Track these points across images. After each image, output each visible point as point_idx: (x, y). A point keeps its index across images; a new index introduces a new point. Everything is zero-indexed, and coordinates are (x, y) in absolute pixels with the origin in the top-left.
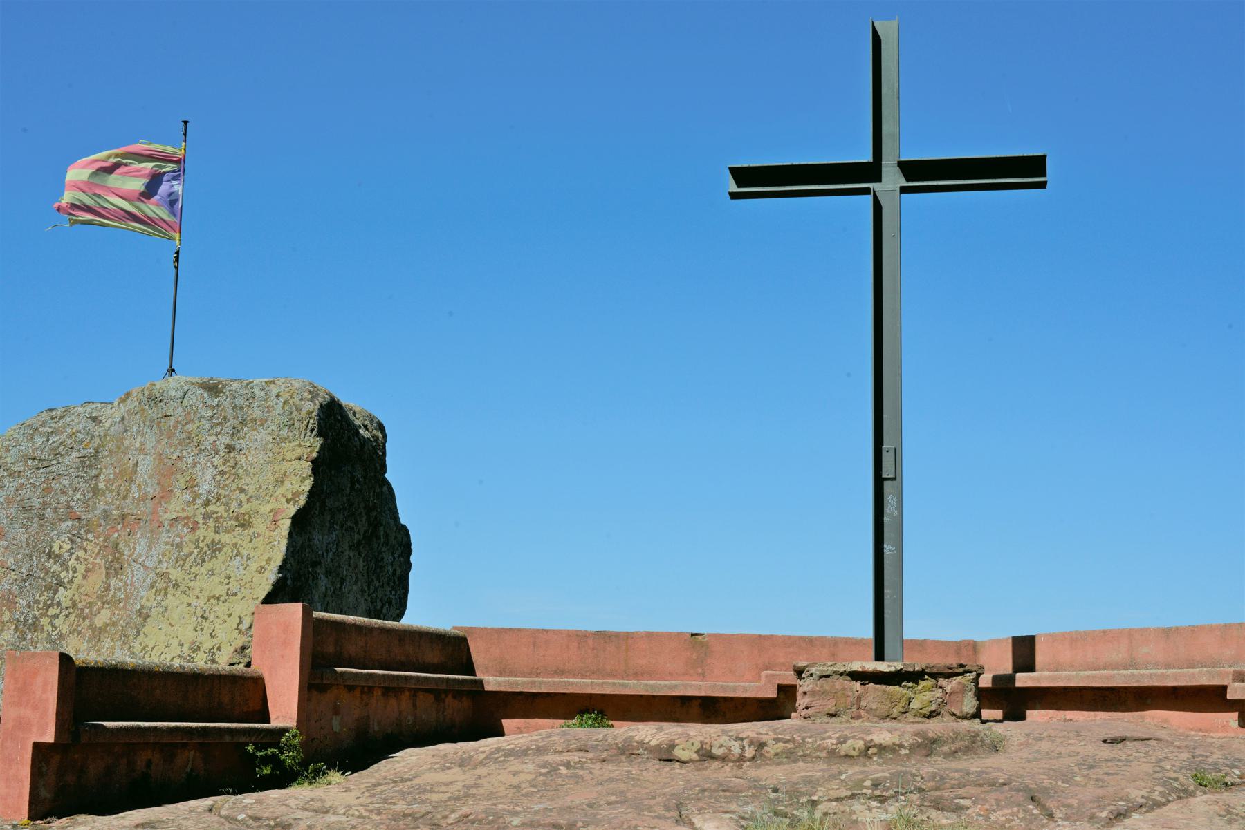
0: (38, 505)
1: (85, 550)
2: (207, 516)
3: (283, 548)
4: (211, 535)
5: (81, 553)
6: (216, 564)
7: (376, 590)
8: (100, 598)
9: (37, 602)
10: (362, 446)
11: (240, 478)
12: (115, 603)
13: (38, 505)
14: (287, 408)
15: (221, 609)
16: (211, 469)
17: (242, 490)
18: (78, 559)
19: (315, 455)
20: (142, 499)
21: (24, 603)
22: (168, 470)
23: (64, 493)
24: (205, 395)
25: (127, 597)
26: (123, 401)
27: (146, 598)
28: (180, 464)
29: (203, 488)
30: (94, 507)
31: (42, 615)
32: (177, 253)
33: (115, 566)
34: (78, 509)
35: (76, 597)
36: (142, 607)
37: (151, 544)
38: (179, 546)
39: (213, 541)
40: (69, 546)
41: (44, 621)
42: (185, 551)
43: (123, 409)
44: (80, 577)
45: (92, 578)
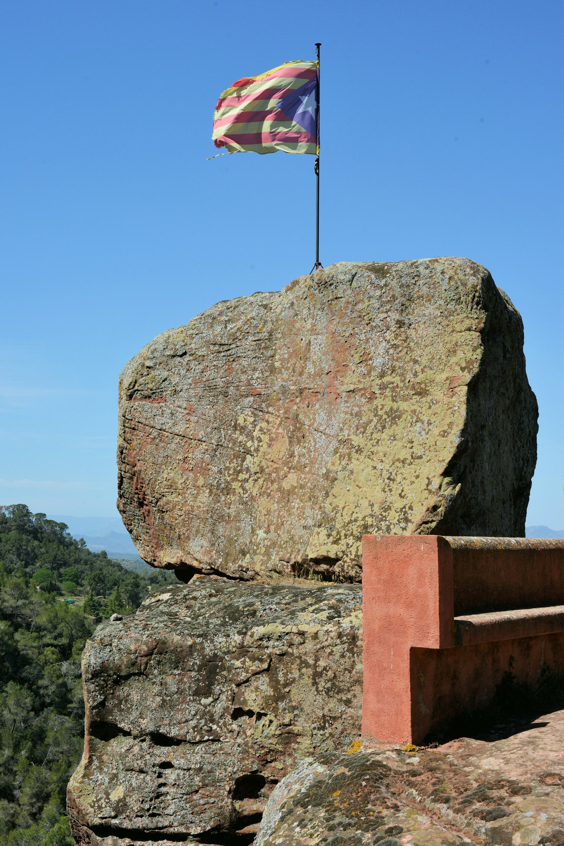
0: (221, 384)
1: (268, 422)
2: (383, 387)
3: (464, 413)
4: (389, 404)
5: (264, 425)
6: (398, 429)
7: (519, 450)
8: (286, 463)
9: (227, 468)
10: (510, 318)
11: (412, 350)
12: (300, 468)
13: (221, 384)
14: (452, 283)
15: (407, 471)
16: (384, 344)
17: (416, 362)
18: (261, 430)
19: (482, 325)
20: (319, 374)
21: (216, 469)
22: (341, 346)
23: (244, 372)
24: (373, 276)
25: (312, 462)
26: (289, 289)
27: (331, 462)
28: (352, 340)
29: (378, 362)
30: (273, 383)
31: (233, 480)
32: (318, 160)
33: (297, 434)
34: (259, 388)
35: (263, 464)
36: (328, 471)
37: (330, 415)
38: (358, 415)
39: (391, 409)
40: (252, 419)
41: (235, 485)
42: (364, 419)
43: (291, 296)
44: (265, 446)
45: (277, 446)
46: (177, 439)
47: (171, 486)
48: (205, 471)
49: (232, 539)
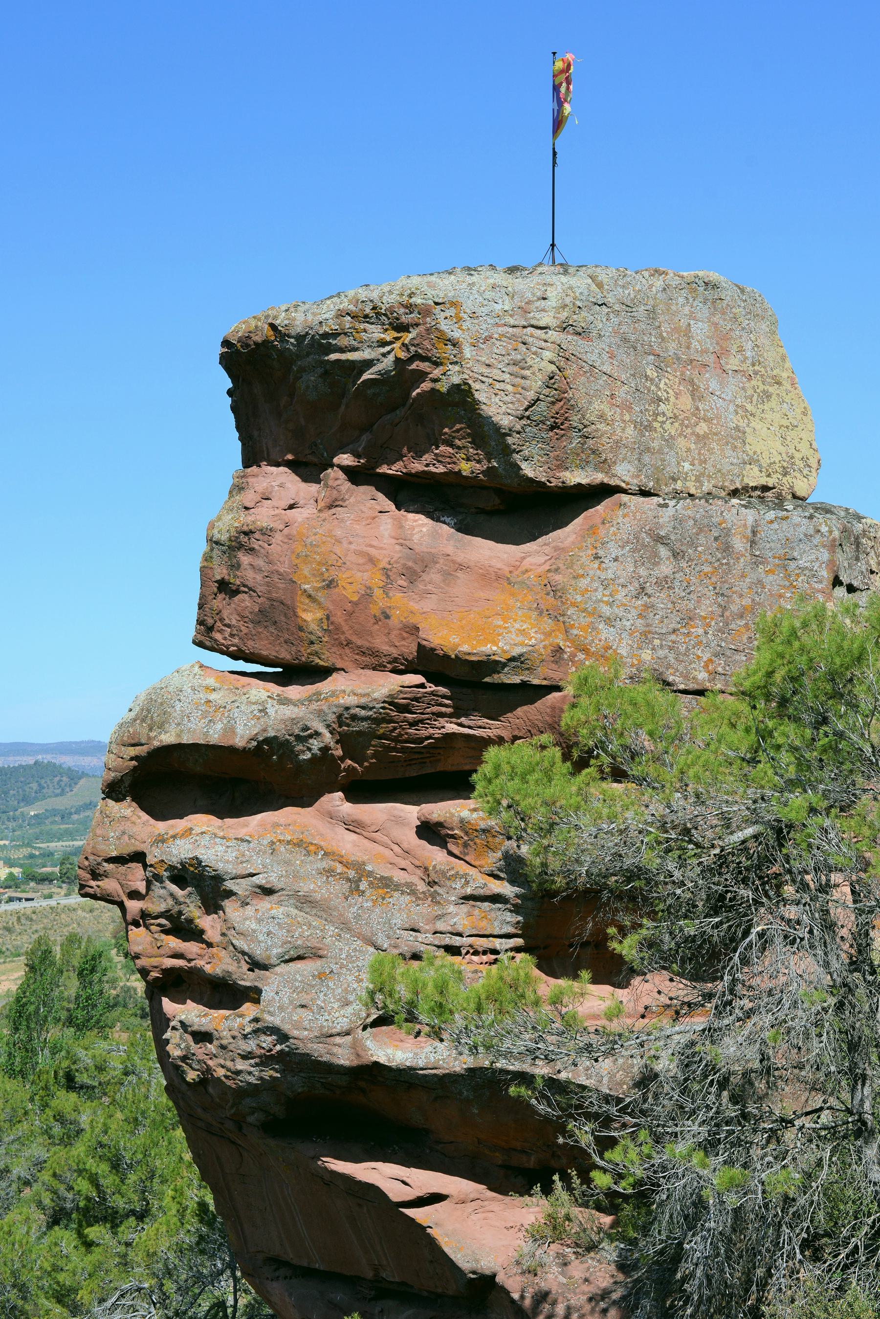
8: (694, 415)
9: (646, 410)
16: (750, 342)
21: (637, 409)
34: (658, 350)
41: (656, 425)
46: (605, 378)
47: (602, 417)
48: (629, 409)
49: (658, 467)
